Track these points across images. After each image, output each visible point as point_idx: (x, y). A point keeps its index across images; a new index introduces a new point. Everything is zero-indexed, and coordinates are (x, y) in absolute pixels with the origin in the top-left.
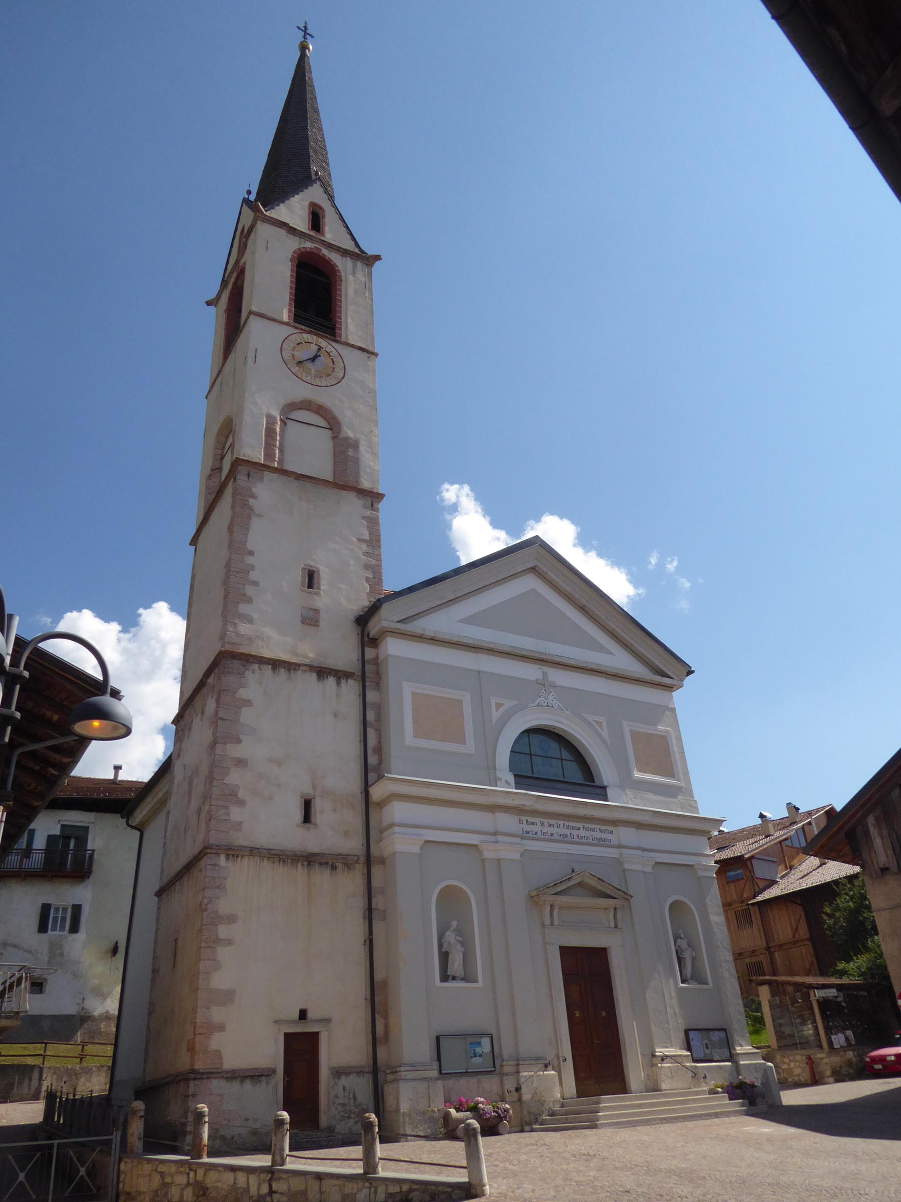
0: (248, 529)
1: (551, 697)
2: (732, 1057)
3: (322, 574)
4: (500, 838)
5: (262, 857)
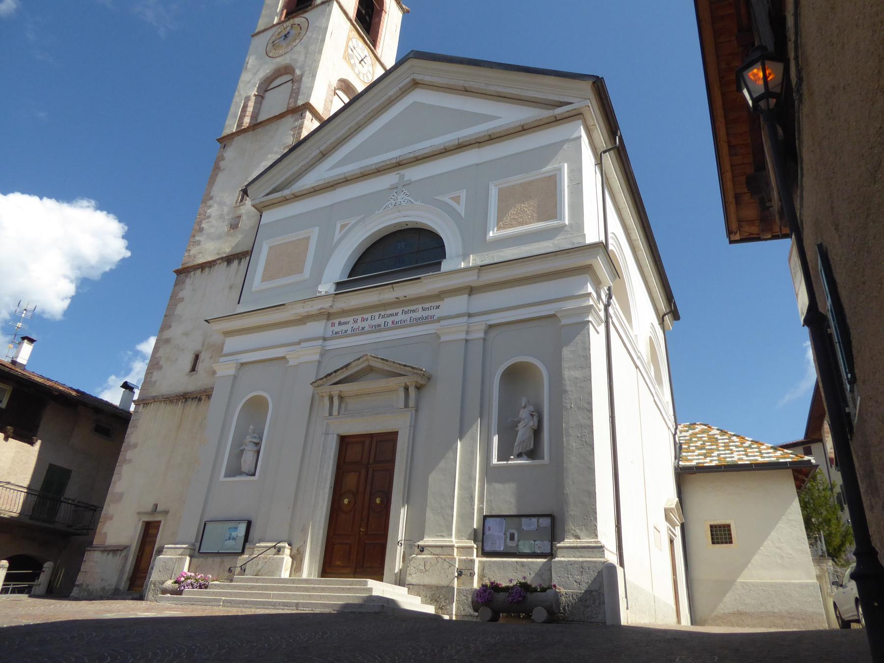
4: (303, 345)
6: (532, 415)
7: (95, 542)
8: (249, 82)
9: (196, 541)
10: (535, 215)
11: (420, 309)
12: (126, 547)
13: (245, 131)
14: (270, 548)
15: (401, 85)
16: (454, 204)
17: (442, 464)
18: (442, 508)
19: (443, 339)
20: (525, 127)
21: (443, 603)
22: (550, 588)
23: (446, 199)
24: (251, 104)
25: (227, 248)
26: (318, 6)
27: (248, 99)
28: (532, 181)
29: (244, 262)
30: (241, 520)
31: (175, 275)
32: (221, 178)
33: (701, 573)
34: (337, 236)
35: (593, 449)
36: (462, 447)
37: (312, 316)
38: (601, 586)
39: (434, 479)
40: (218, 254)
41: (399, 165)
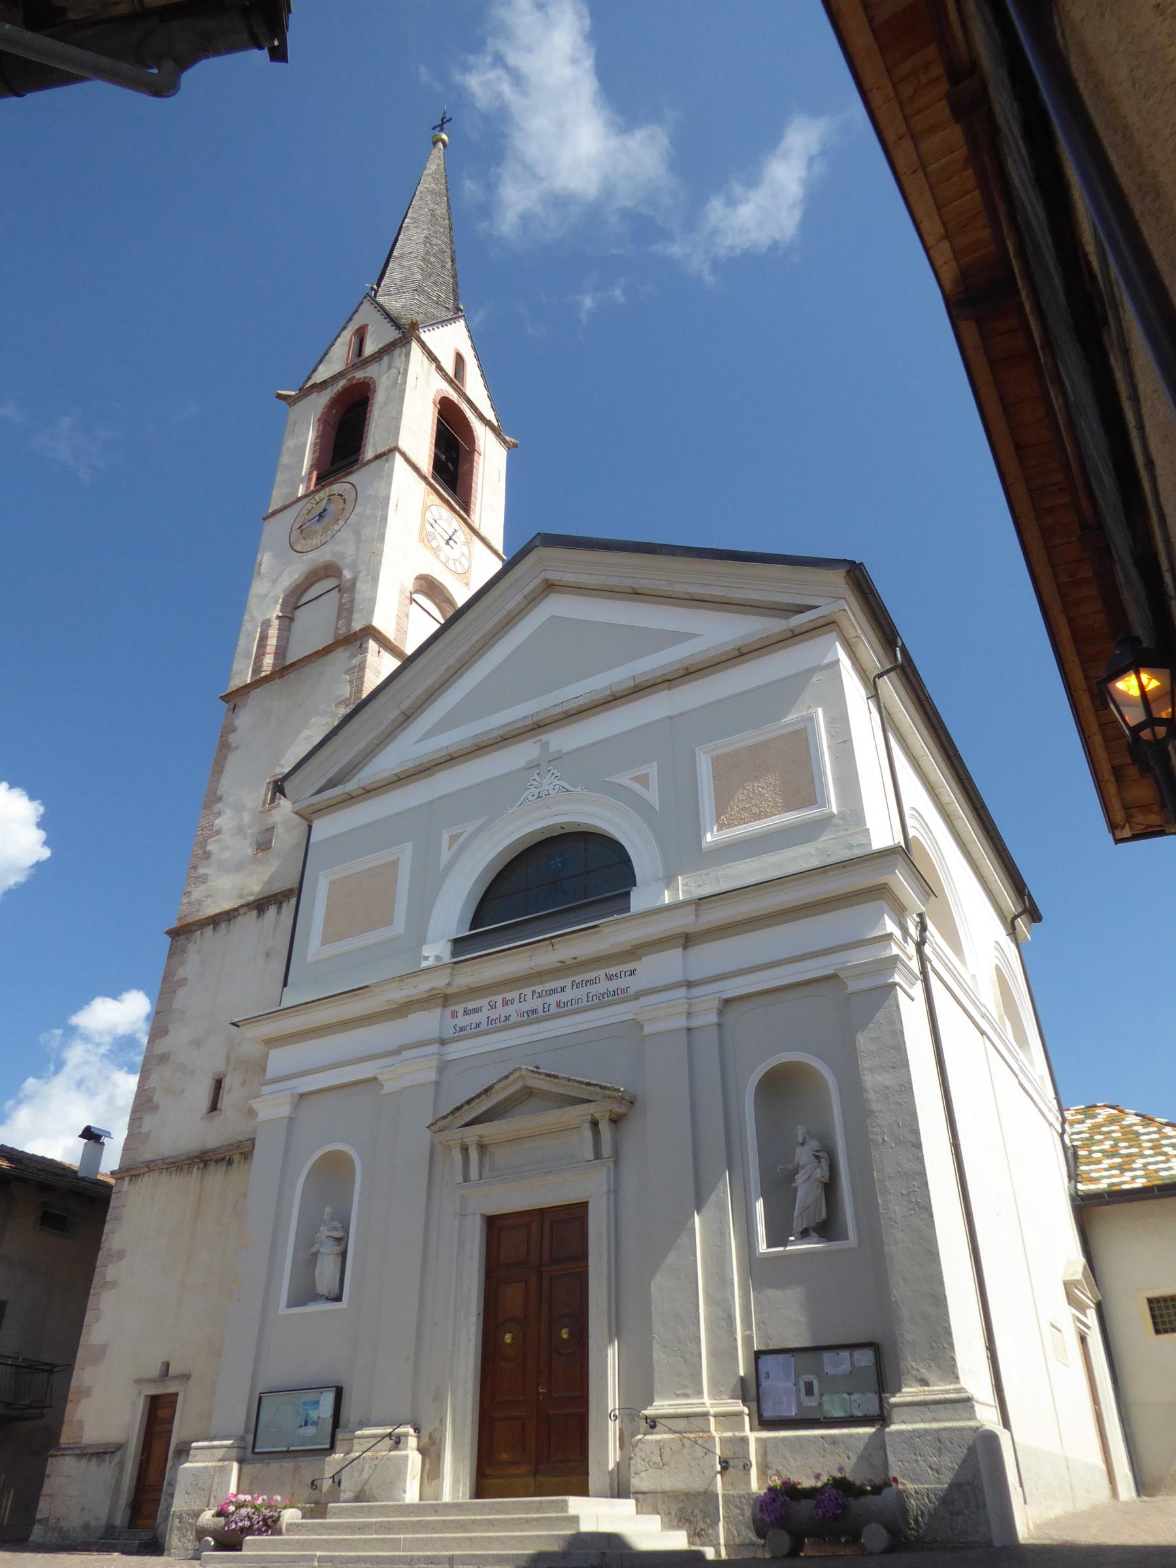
4: (407, 1054)
5: (160, 1170)
6: (817, 1157)
7: (64, 1440)
8: (265, 596)
9: (247, 1431)
10: (779, 800)
11: (603, 978)
12: (119, 1447)
13: (267, 679)
14: (383, 1437)
15: (526, 591)
16: (637, 788)
17: (671, 1259)
19: (648, 1029)
20: (743, 651)
21: (701, 1525)
22: (887, 1484)
23: (624, 779)
24: (273, 633)
25: (255, 885)
26: (369, 462)
27: (266, 624)
28: (766, 742)
29: (288, 908)
30: (323, 1388)
31: (168, 939)
32: (233, 762)
33: (1141, 1389)
34: (446, 855)
35: (931, 1215)
36: (702, 1224)
37: (417, 1002)
39: (661, 1285)
40: (241, 896)
41: (537, 727)
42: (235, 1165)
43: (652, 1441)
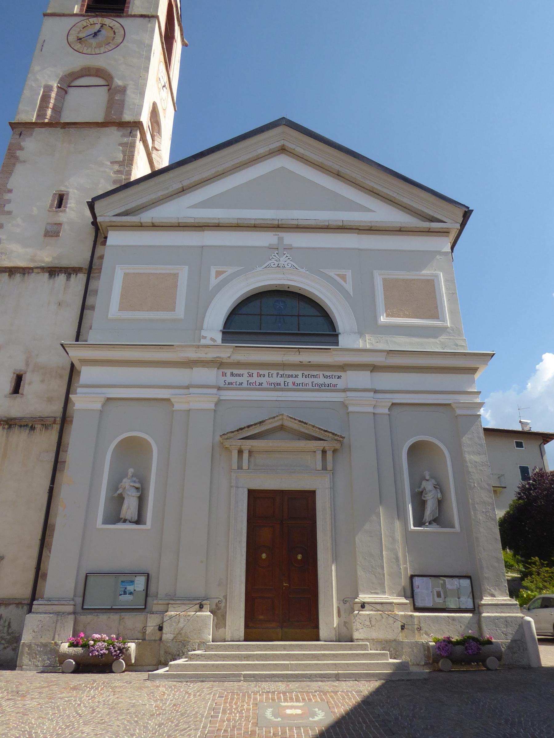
0: (11, 174)
1: (283, 259)
2: (475, 609)
3: (70, 195)
4: (192, 390)
18: (372, 567)
19: (351, 409)
23: (332, 273)
38: (523, 635)
40: (33, 260)
41: (278, 227)
42: (37, 431)
43: (364, 615)
